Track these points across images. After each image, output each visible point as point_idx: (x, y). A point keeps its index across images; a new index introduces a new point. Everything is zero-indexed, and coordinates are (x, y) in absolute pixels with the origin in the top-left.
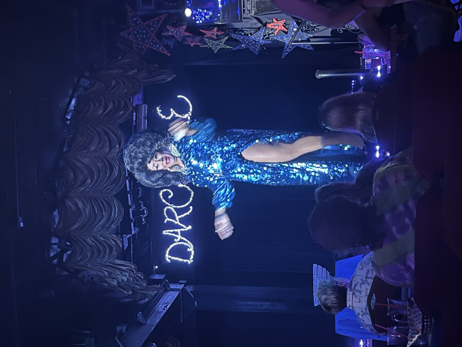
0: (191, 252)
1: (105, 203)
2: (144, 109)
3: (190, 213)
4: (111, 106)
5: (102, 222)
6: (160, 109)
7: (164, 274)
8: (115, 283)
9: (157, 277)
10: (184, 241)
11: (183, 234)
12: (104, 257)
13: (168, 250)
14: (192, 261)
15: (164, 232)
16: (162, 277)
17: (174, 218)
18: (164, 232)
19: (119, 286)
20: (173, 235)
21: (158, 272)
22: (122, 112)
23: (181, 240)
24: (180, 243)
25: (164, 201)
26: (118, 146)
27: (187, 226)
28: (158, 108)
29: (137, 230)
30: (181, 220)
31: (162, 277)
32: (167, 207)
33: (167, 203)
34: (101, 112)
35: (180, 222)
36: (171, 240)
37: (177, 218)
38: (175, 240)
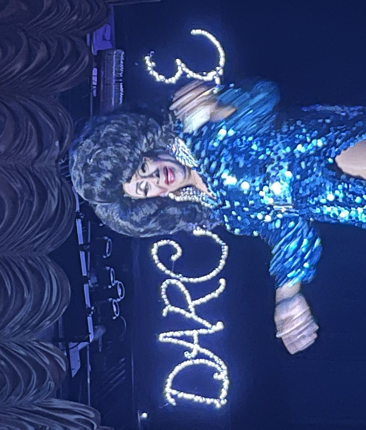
1: (28, 272)
2: (117, 61)
3: (221, 294)
4: (41, 54)
5: (22, 314)
6: (151, 60)
10: (207, 358)
11: (204, 341)
12: (26, 393)
13: (171, 376)
14: (224, 402)
17: (185, 306)
20: (181, 342)
22: (66, 68)
24: (197, 362)
25: (161, 266)
26: (57, 143)
27: (213, 323)
28: (147, 58)
29: (101, 331)
30: (199, 310)
32: (167, 281)
34: (19, 66)
35: (197, 314)
36: (177, 354)
37: (191, 304)
38: (187, 355)
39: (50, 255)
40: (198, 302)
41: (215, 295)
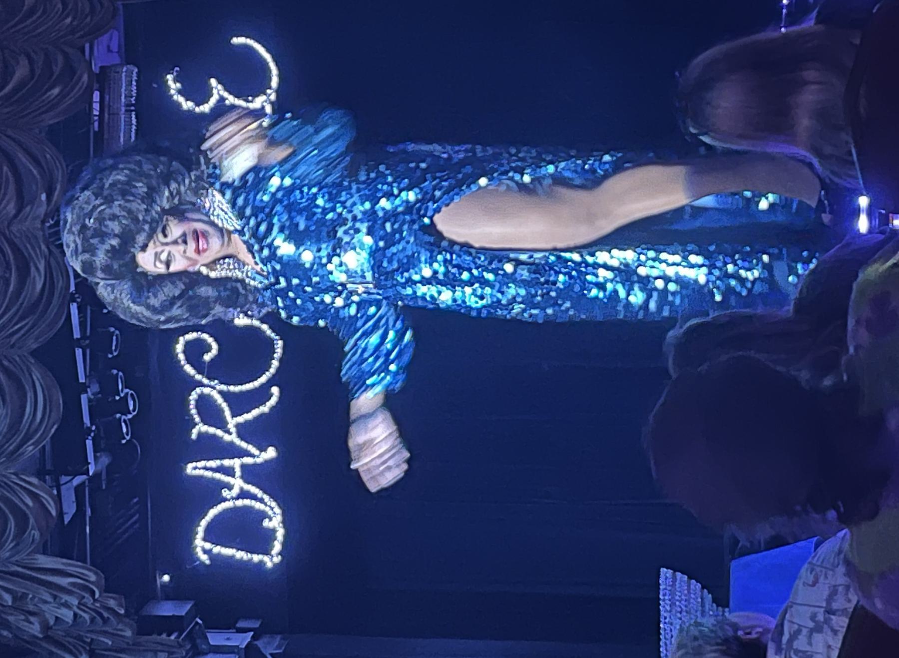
0: (274, 531)
3: (273, 408)
6: (176, 80)
7: (188, 599)
8: (35, 628)
9: (167, 609)
10: (254, 497)
11: (249, 473)
13: (204, 523)
14: (277, 559)
15: (190, 469)
16: (182, 609)
17: (222, 424)
18: (190, 469)
19: (47, 638)
20: (218, 476)
21: (172, 594)
22: (56, 91)
23: (243, 494)
24: (240, 503)
25: (188, 369)
26: (44, 197)
27: (262, 449)
28: (170, 77)
29: (105, 460)
30: (244, 431)
31: (182, 609)
32: (198, 390)
33: (198, 377)
35: (240, 436)
36: (211, 492)
37: (232, 422)
38: (225, 493)
39: (34, 353)
40: (240, 419)
41: (265, 409)
